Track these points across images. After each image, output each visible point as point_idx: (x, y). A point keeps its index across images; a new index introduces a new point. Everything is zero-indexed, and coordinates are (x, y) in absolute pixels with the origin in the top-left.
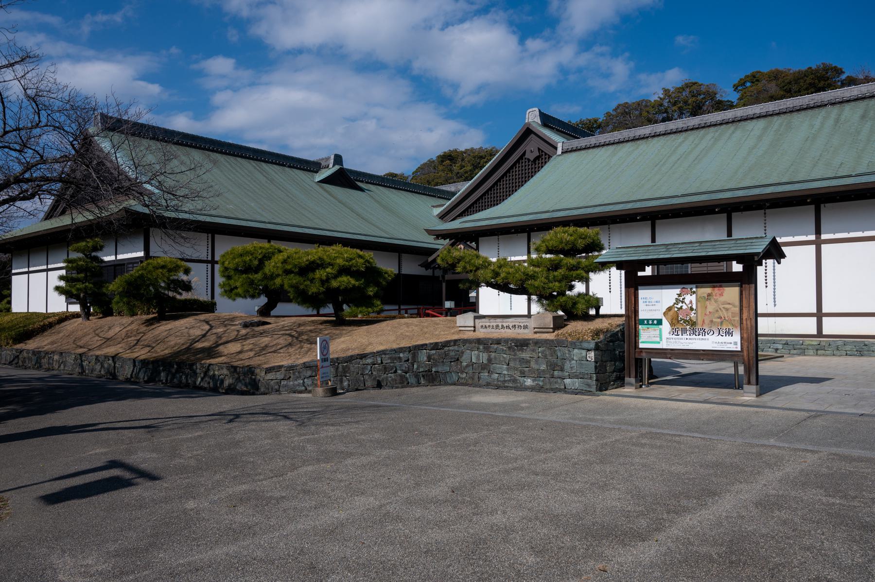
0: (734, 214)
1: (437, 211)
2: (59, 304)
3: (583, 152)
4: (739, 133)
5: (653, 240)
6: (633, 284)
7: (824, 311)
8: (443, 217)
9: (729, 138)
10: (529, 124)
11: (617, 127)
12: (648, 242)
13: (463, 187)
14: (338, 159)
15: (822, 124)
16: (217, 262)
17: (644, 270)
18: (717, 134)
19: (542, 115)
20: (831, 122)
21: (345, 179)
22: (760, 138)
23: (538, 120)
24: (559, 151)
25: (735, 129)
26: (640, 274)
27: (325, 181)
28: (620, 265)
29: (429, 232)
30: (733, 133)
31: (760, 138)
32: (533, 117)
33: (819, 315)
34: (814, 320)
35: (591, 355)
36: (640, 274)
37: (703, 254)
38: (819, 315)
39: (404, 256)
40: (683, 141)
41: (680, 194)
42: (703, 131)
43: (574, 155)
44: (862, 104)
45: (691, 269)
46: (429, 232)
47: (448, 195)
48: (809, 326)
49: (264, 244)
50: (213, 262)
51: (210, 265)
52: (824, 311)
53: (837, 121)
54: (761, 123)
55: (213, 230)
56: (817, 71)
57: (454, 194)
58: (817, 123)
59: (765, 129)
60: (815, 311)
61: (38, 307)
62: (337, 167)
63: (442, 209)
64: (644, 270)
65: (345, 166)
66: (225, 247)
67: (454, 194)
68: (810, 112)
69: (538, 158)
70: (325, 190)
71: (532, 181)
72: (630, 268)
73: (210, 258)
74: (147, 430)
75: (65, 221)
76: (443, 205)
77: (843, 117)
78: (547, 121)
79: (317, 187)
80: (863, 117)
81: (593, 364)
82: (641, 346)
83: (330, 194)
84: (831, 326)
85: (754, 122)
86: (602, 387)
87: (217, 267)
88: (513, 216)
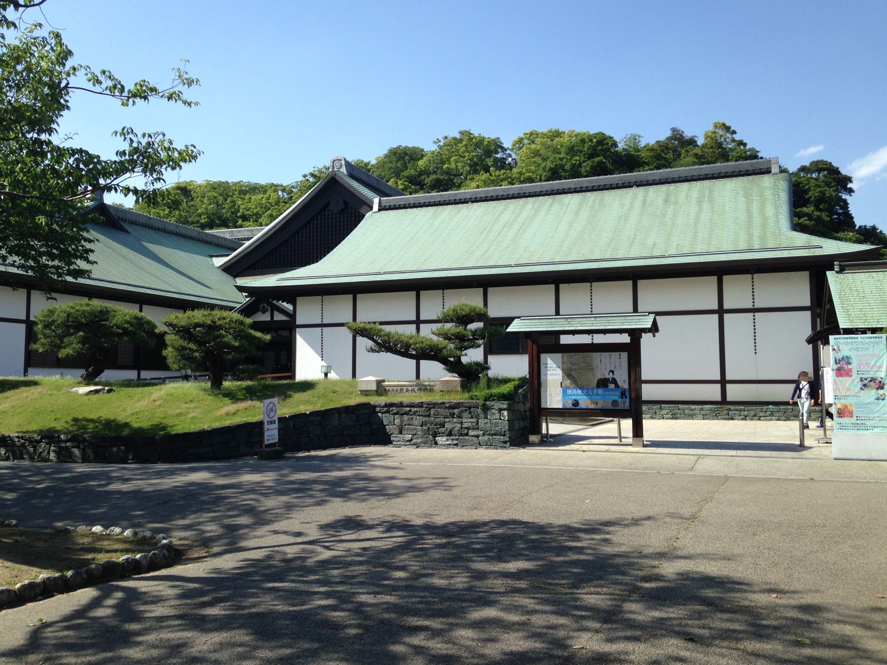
4: (556, 207)
7: (727, 378)
9: (548, 210)
15: (632, 203)
18: (536, 205)
20: (638, 204)
22: (577, 213)
24: (376, 207)
25: (553, 201)
30: (552, 205)
31: (577, 213)
34: (718, 387)
38: (723, 382)
40: (505, 209)
45: (599, 339)
52: (727, 378)
53: (644, 202)
56: (663, 142)
57: (239, 242)
58: (627, 202)
59: (581, 204)
60: (719, 378)
67: (239, 242)
74: (169, 583)
76: (228, 255)
77: (649, 200)
80: (666, 201)
84: (734, 392)
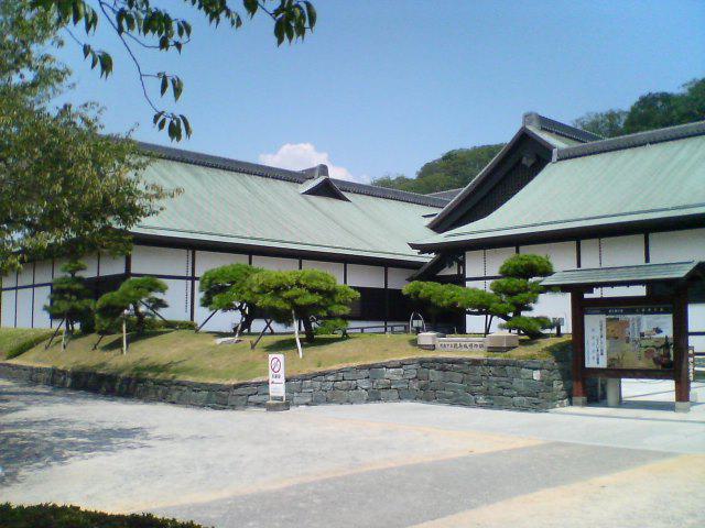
0: (582, 242)
2: (44, 323)
5: (647, 260)
6: (581, 308)
8: (438, 227)
12: (643, 262)
14: (323, 169)
16: (197, 279)
17: (592, 292)
21: (329, 190)
26: (586, 296)
27: (313, 192)
29: (414, 246)
36: (586, 296)
37: (591, 281)
39: (390, 269)
41: (670, 207)
46: (414, 246)
49: (243, 260)
50: (193, 278)
51: (190, 282)
55: (193, 246)
58: (683, 154)
61: (24, 323)
62: (322, 178)
63: (433, 218)
64: (592, 292)
66: (207, 264)
70: (310, 203)
72: (577, 291)
73: (190, 275)
79: (301, 199)
83: (314, 205)
87: (197, 283)
88: (652, 211)
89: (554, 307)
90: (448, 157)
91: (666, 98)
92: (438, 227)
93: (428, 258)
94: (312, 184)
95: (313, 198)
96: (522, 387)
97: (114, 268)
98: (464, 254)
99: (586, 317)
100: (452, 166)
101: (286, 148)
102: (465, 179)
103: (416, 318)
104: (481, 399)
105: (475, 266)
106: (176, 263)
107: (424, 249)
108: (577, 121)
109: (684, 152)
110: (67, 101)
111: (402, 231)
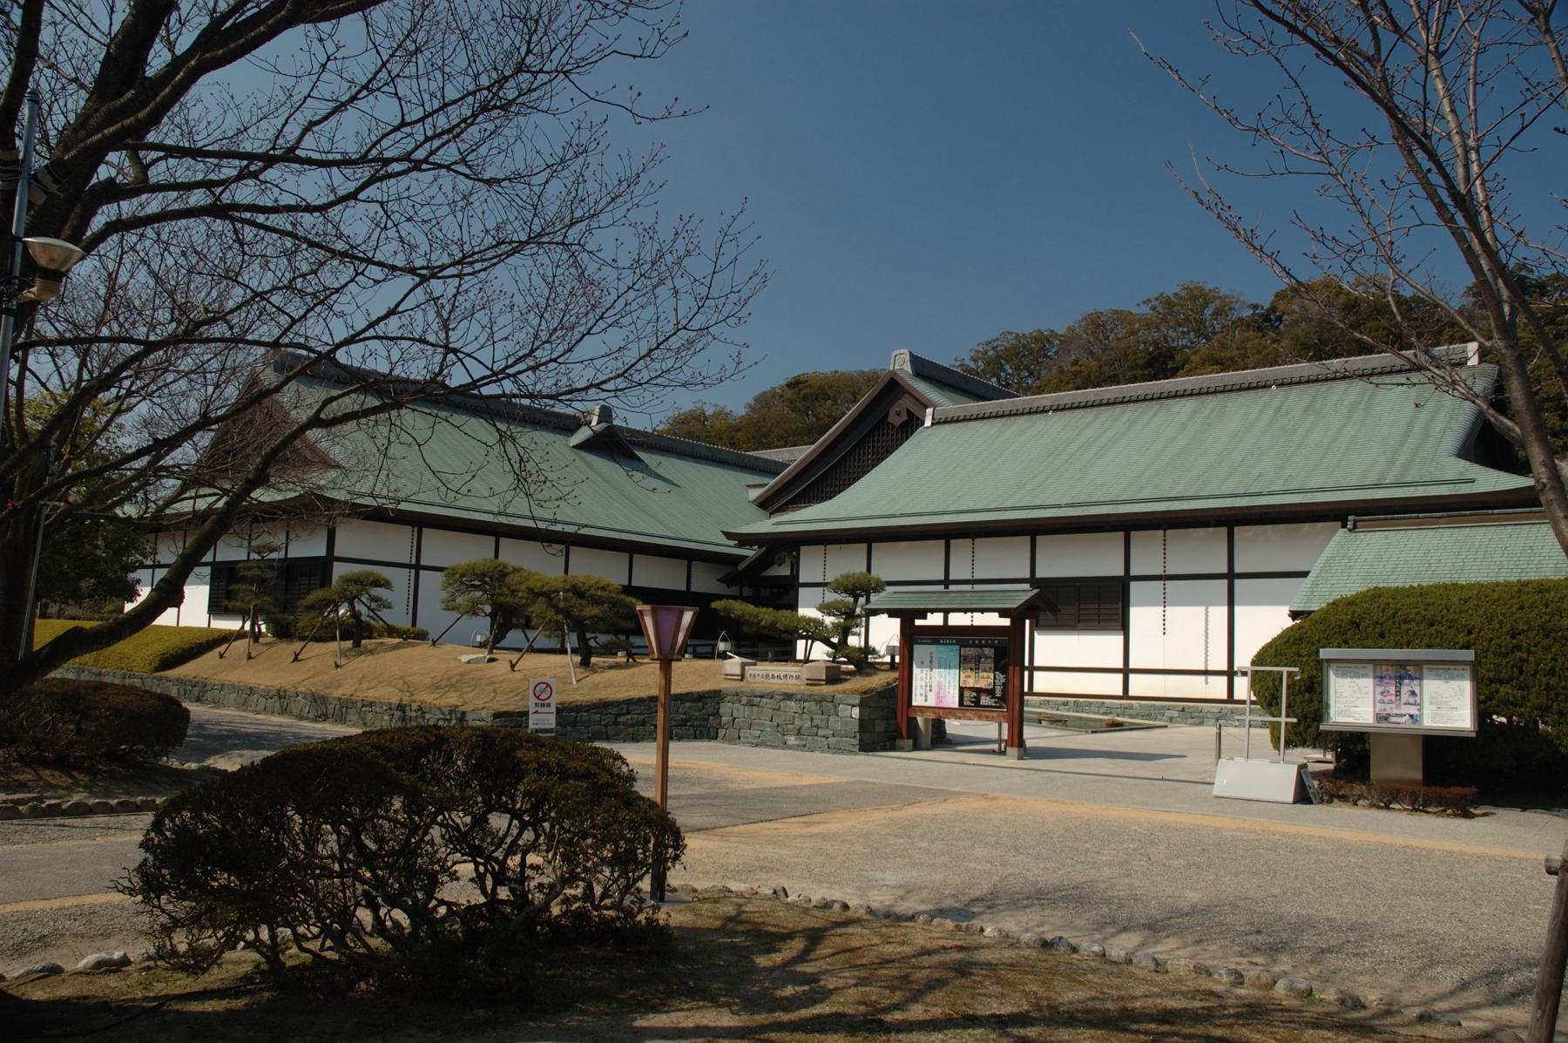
0: (874, 545)
1: (754, 494)
3: (959, 425)
6: (911, 636)
10: (894, 372)
11: (421, 750)
13: (799, 454)
15: (1261, 412)
17: (925, 617)
19: (915, 360)
23: (908, 368)
24: (928, 423)
26: (918, 622)
27: (583, 446)
28: (892, 613)
29: (729, 535)
32: (901, 365)
33: (1126, 671)
35: (856, 712)
36: (918, 622)
42: (1119, 408)
43: (947, 428)
44: (1311, 389)
46: (729, 535)
47: (770, 469)
48: (1113, 684)
53: (1278, 410)
54: (1191, 404)
57: (785, 466)
59: (1194, 413)
62: (604, 425)
63: (760, 491)
64: (925, 617)
65: (616, 422)
68: (1252, 394)
69: (904, 424)
71: (901, 448)
75: (18, 259)
78: (924, 369)
79: (572, 455)
81: (857, 723)
82: (1043, 682)
85: (1184, 401)
86: (867, 746)
89: (884, 633)
90: (795, 384)
91: (1121, 317)
92: (770, 504)
93: (750, 553)
94: (583, 434)
95: (586, 455)
96: (838, 726)
97: (309, 547)
98: (798, 552)
99: (916, 647)
100: (805, 399)
101: (257, 761)
102: (1116, 376)
103: (724, 639)
104: (792, 740)
105: (811, 567)
106: (394, 544)
107: (744, 540)
108: (988, 344)
109: (1125, 418)
110: (786, 883)
111: (713, 508)
